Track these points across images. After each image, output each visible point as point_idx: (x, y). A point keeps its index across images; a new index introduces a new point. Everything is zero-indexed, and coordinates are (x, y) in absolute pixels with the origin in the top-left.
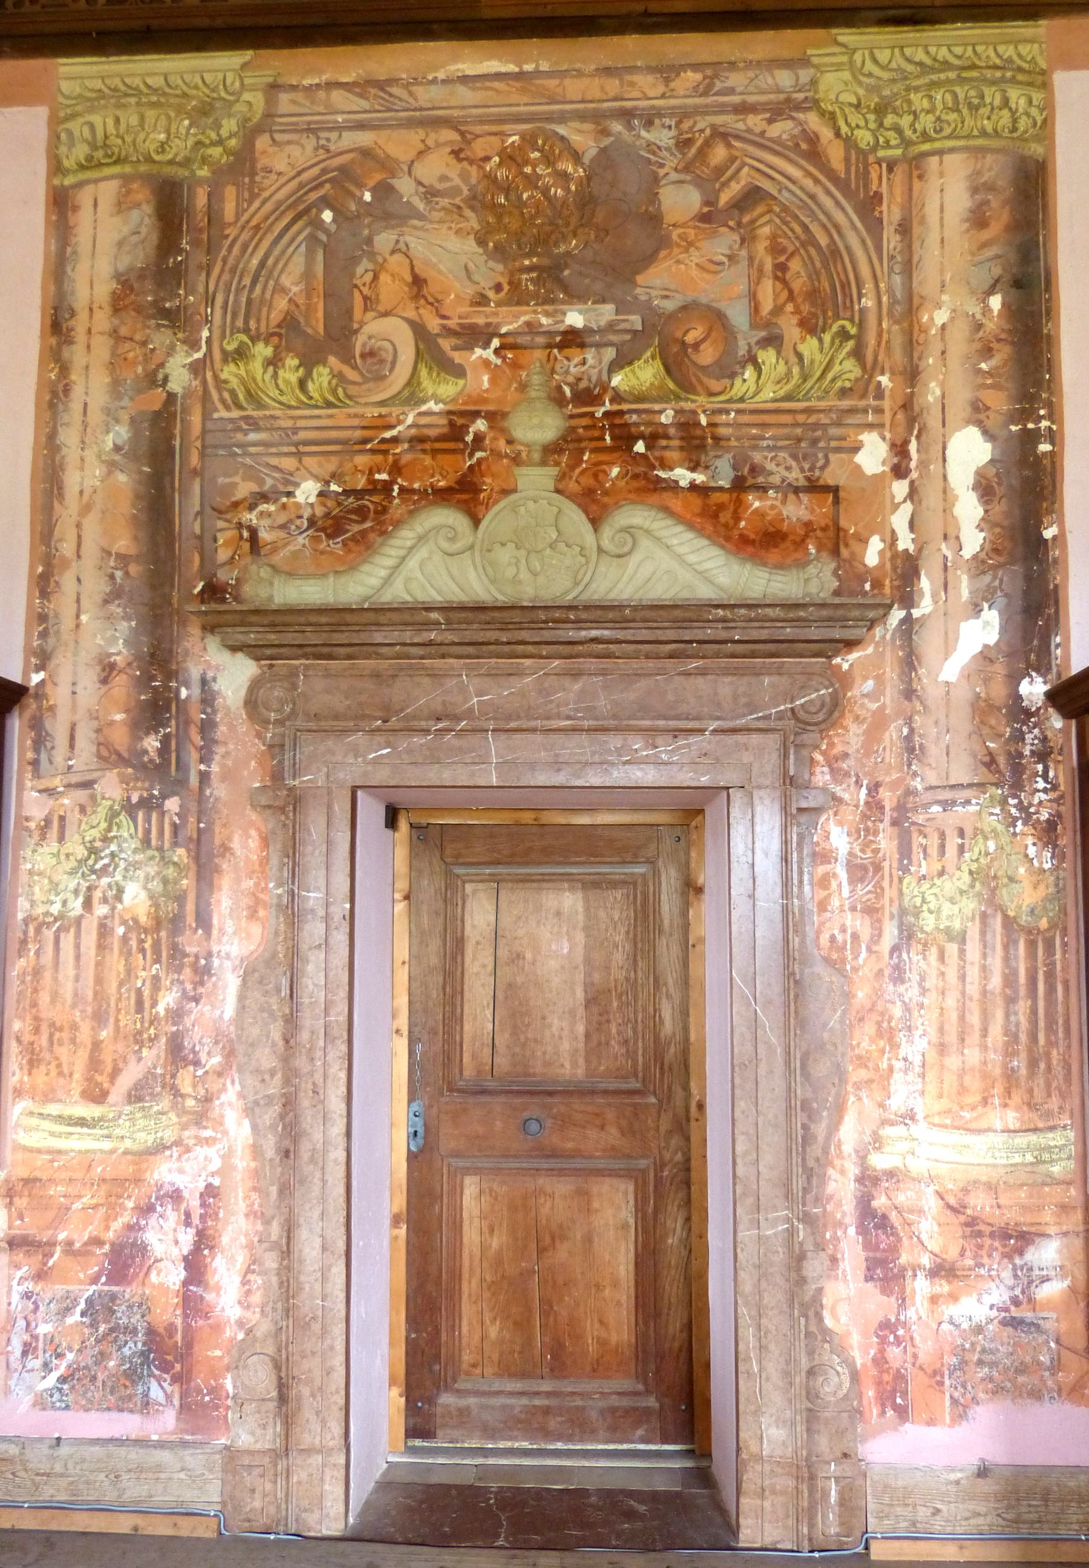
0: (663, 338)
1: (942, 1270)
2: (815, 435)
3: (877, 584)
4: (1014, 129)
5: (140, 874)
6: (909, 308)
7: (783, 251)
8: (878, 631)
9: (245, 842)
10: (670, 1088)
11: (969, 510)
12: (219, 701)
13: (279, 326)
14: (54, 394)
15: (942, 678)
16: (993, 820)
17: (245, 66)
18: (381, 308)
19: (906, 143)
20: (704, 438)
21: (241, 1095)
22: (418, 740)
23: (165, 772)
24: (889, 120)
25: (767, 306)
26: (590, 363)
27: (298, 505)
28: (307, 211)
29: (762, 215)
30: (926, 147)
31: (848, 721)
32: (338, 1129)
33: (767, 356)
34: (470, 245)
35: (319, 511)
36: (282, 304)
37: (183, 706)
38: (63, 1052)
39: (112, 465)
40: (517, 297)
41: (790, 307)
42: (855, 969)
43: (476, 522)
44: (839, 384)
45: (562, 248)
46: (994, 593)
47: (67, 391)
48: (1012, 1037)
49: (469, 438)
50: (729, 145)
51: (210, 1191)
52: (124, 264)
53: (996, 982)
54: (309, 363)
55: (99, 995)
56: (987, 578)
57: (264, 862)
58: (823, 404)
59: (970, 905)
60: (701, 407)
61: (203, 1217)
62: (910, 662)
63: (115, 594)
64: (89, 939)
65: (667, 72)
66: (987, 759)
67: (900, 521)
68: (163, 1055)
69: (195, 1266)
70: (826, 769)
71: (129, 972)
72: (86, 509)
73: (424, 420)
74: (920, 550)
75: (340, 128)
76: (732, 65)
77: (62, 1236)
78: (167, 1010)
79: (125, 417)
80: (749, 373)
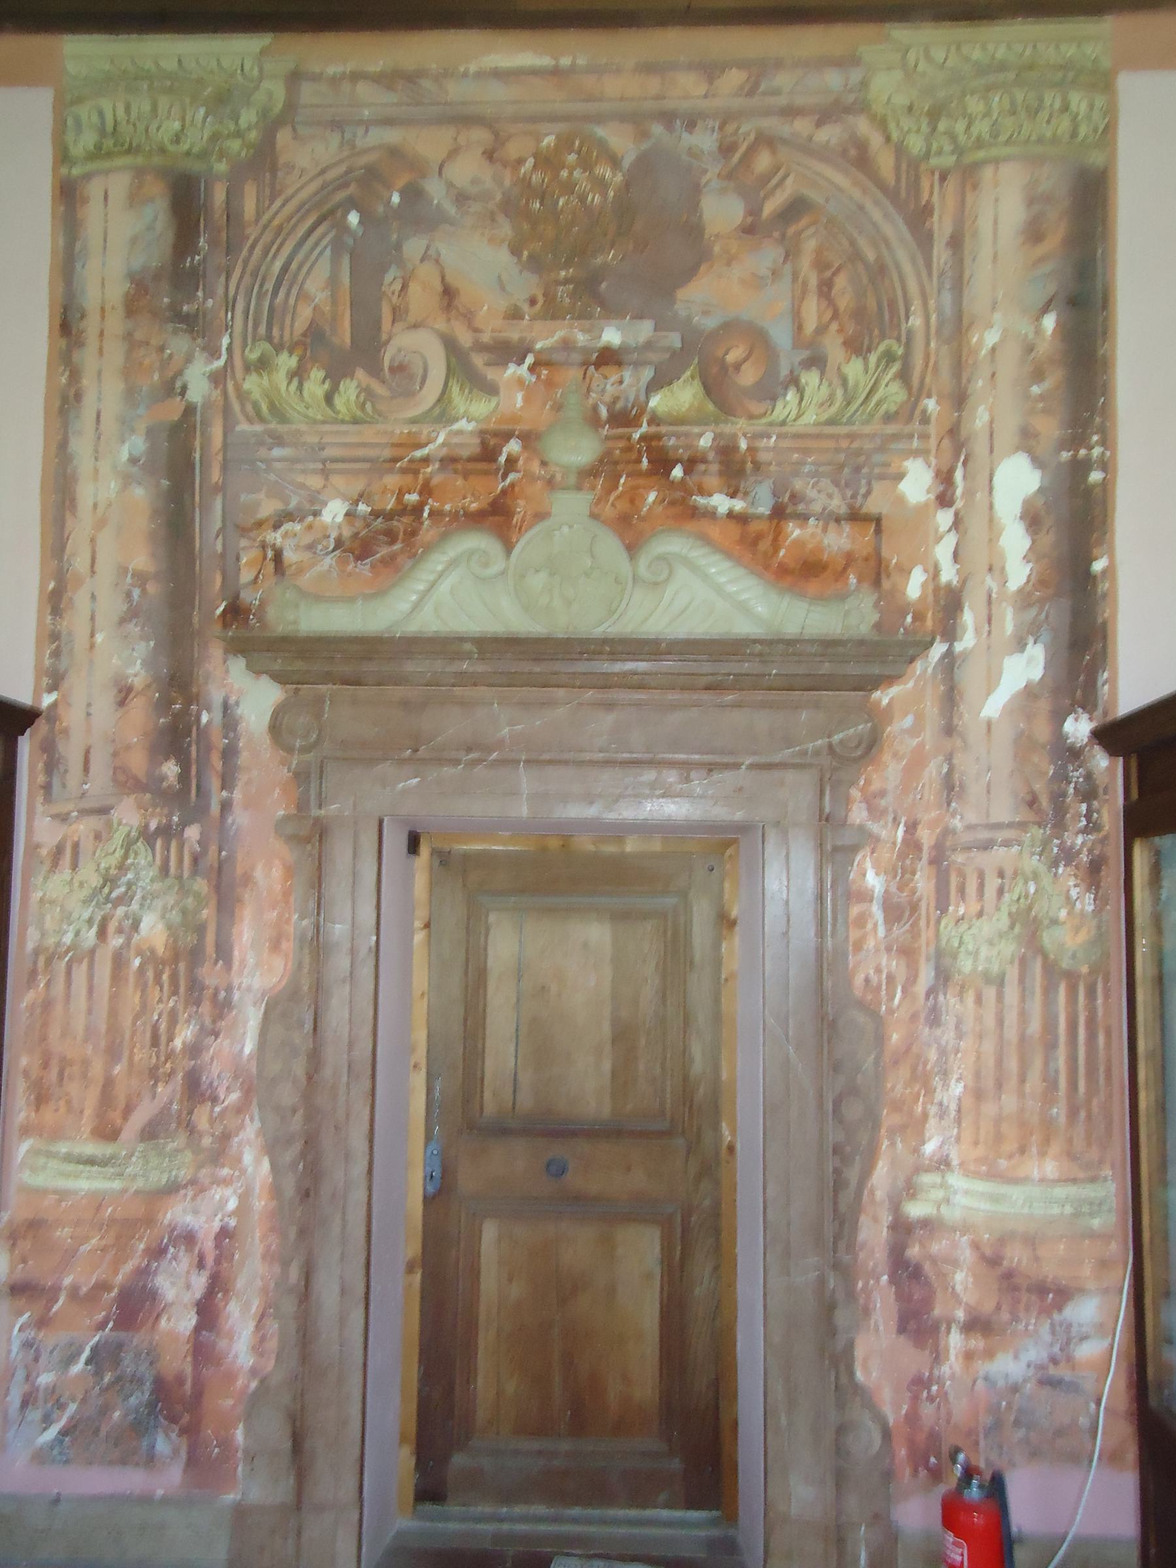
0: (701, 357)
1: (976, 1325)
2: (858, 464)
3: (919, 617)
4: (1074, 134)
5: (159, 904)
6: (958, 328)
7: (828, 266)
8: (918, 666)
9: (268, 870)
10: (699, 1129)
11: (1015, 541)
12: (242, 727)
13: (304, 335)
14: (65, 400)
15: (983, 714)
16: (1033, 863)
17: (263, 52)
18: (411, 318)
19: (959, 151)
20: (744, 462)
21: (261, 1132)
22: (448, 771)
23: (186, 800)
24: (942, 126)
25: (810, 326)
26: (628, 383)
27: (325, 527)
28: (332, 212)
29: (808, 227)
30: (981, 154)
31: (886, 757)
32: (359, 1168)
33: (810, 379)
34: (504, 256)
35: (347, 533)
36: (305, 313)
37: (203, 733)
38: (73, 1088)
39: (127, 480)
40: (552, 311)
41: (834, 327)
42: (891, 1011)
43: (509, 547)
44: (884, 407)
45: (599, 260)
46: (1039, 627)
47: (78, 397)
48: (1051, 1083)
49: (502, 459)
50: (774, 152)
51: (224, 1234)
52: (137, 263)
53: (1035, 1026)
54: (335, 376)
55: (113, 1028)
56: (1033, 612)
57: (286, 894)
58: (867, 429)
59: (1009, 948)
60: (741, 431)
61: (218, 1261)
62: (951, 698)
63: (132, 614)
64: (104, 970)
65: (711, 70)
66: (1029, 798)
67: (943, 552)
68: (179, 1088)
69: (208, 1312)
70: (864, 805)
71: (144, 1005)
72: (101, 524)
73: (455, 440)
74: (964, 582)
75: (367, 124)
76: (779, 64)
77: (67, 1281)
78: (184, 1043)
79: (142, 427)
80: (791, 396)
